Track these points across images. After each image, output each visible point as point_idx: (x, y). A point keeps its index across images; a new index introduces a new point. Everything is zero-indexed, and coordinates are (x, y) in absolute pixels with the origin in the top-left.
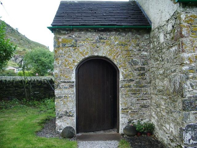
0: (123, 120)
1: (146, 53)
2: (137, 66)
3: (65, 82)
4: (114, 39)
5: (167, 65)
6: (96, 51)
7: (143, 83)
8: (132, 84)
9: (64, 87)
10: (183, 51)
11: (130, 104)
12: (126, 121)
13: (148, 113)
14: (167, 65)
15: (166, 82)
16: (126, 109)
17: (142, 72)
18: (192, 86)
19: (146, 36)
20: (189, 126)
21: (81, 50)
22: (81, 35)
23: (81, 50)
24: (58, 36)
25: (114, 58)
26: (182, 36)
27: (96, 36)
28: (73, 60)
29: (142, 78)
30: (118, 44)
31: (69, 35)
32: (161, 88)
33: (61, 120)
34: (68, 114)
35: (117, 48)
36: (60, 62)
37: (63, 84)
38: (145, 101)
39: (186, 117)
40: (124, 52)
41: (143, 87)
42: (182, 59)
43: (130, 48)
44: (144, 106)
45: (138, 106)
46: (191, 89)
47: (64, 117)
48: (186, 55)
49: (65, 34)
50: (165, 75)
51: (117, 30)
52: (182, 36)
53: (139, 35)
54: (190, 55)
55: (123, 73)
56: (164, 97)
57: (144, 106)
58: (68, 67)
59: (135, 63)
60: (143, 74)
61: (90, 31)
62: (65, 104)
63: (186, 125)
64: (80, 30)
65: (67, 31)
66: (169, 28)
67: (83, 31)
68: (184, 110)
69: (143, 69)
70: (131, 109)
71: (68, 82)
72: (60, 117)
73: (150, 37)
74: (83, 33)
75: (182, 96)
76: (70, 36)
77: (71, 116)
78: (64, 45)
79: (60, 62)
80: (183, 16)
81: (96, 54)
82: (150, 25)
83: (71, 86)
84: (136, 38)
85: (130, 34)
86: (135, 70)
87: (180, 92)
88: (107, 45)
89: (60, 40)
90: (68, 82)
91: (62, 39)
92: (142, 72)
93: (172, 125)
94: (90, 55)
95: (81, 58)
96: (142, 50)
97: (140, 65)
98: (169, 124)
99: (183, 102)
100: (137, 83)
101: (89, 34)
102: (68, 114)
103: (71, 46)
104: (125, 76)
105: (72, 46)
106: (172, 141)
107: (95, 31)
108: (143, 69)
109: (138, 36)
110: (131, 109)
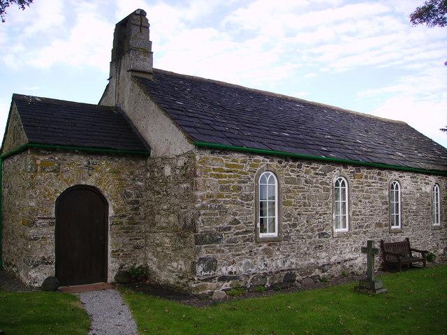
0: (113, 265)
1: (140, 184)
2: (130, 199)
3: (43, 218)
4: (104, 164)
5: (173, 200)
6: (84, 179)
7: (137, 219)
8: (124, 220)
9: (43, 225)
10: (197, 190)
11: (121, 245)
12: (118, 266)
13: (142, 255)
14: (173, 200)
15: (172, 218)
16: (116, 251)
17: (135, 206)
18: (203, 222)
19: (142, 163)
20: (201, 259)
21: (65, 177)
22: (65, 157)
23: (65, 177)
24: (36, 157)
25: (105, 189)
26: (196, 176)
27: (83, 161)
28: (56, 190)
29: (136, 214)
30: (110, 172)
31: (50, 156)
32: (165, 225)
33: (37, 269)
34: (45, 261)
35: (108, 176)
36: (38, 191)
37: (41, 221)
38: (138, 241)
39: (198, 251)
40: (117, 182)
41: (137, 223)
42: (196, 197)
43: (124, 176)
44: (137, 247)
45: (130, 248)
46: (202, 225)
47: (40, 266)
48: (199, 194)
49: (45, 154)
50: (169, 212)
51: (108, 154)
52: (196, 176)
53: (134, 161)
54: (202, 193)
55: (114, 207)
56: (169, 234)
57: (137, 247)
58: (48, 199)
59: (129, 195)
60: (137, 209)
61: (77, 153)
62: (42, 247)
63: (198, 258)
64: (65, 151)
65: (48, 150)
66: (180, 163)
67: (68, 152)
68: (196, 244)
69: (137, 202)
70: (122, 251)
71: (48, 218)
72: (35, 266)
73: (146, 165)
74: (68, 154)
75: (195, 231)
76: (51, 158)
77: (50, 264)
78: (43, 170)
79: (38, 191)
80: (197, 158)
81: (83, 183)
82: (148, 151)
83: (51, 224)
84: (131, 164)
85: (124, 159)
86: (128, 203)
87: (193, 227)
88: (97, 171)
89: (38, 162)
90: (48, 218)
91: (41, 161)
92: (135, 206)
93: (181, 262)
94: (76, 184)
95: (65, 187)
96: (137, 179)
97: (133, 197)
98: (177, 261)
99: (196, 237)
100: (130, 219)
101: (76, 157)
102: (45, 261)
103: (52, 171)
104: (117, 211)
105: (54, 171)
106: (181, 278)
107: (84, 154)
108: (137, 202)
109: (133, 162)
110: (122, 251)
